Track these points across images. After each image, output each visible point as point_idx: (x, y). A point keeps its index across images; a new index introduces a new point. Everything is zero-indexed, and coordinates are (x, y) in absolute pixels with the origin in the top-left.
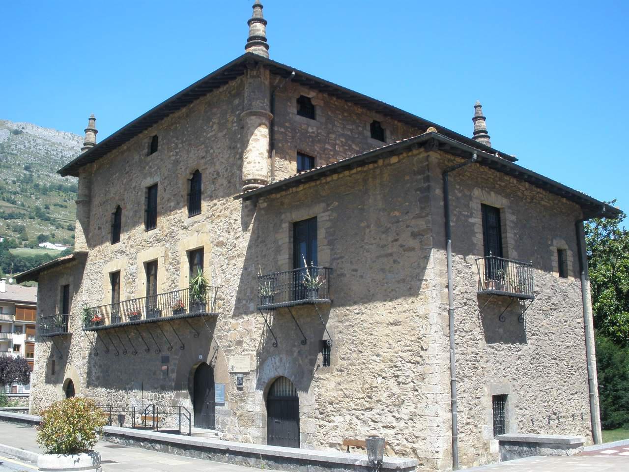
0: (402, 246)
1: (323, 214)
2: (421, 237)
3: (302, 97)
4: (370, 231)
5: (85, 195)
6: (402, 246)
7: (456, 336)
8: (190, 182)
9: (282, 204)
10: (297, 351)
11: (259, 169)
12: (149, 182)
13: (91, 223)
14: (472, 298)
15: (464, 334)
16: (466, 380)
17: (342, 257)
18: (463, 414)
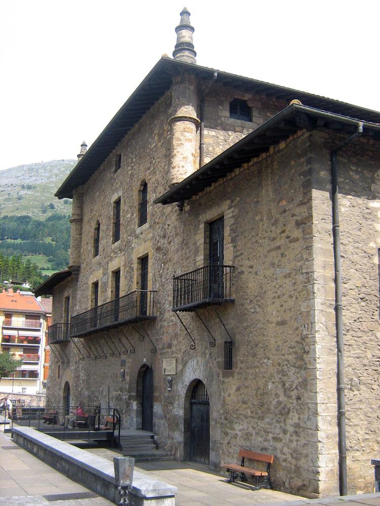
0: (288, 237)
1: (228, 212)
2: (304, 225)
3: (235, 100)
4: (263, 225)
5: (78, 215)
6: (288, 237)
7: (349, 337)
8: (141, 193)
9: (200, 205)
10: (209, 353)
11: (182, 173)
12: (115, 197)
13: (83, 239)
14: (372, 292)
15: (360, 334)
16: (362, 387)
17: (241, 254)
18: (358, 428)
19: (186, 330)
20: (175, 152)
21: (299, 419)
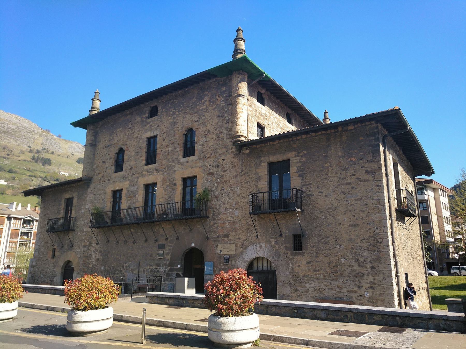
19: (257, 233)
20: (239, 116)
21: (374, 279)
